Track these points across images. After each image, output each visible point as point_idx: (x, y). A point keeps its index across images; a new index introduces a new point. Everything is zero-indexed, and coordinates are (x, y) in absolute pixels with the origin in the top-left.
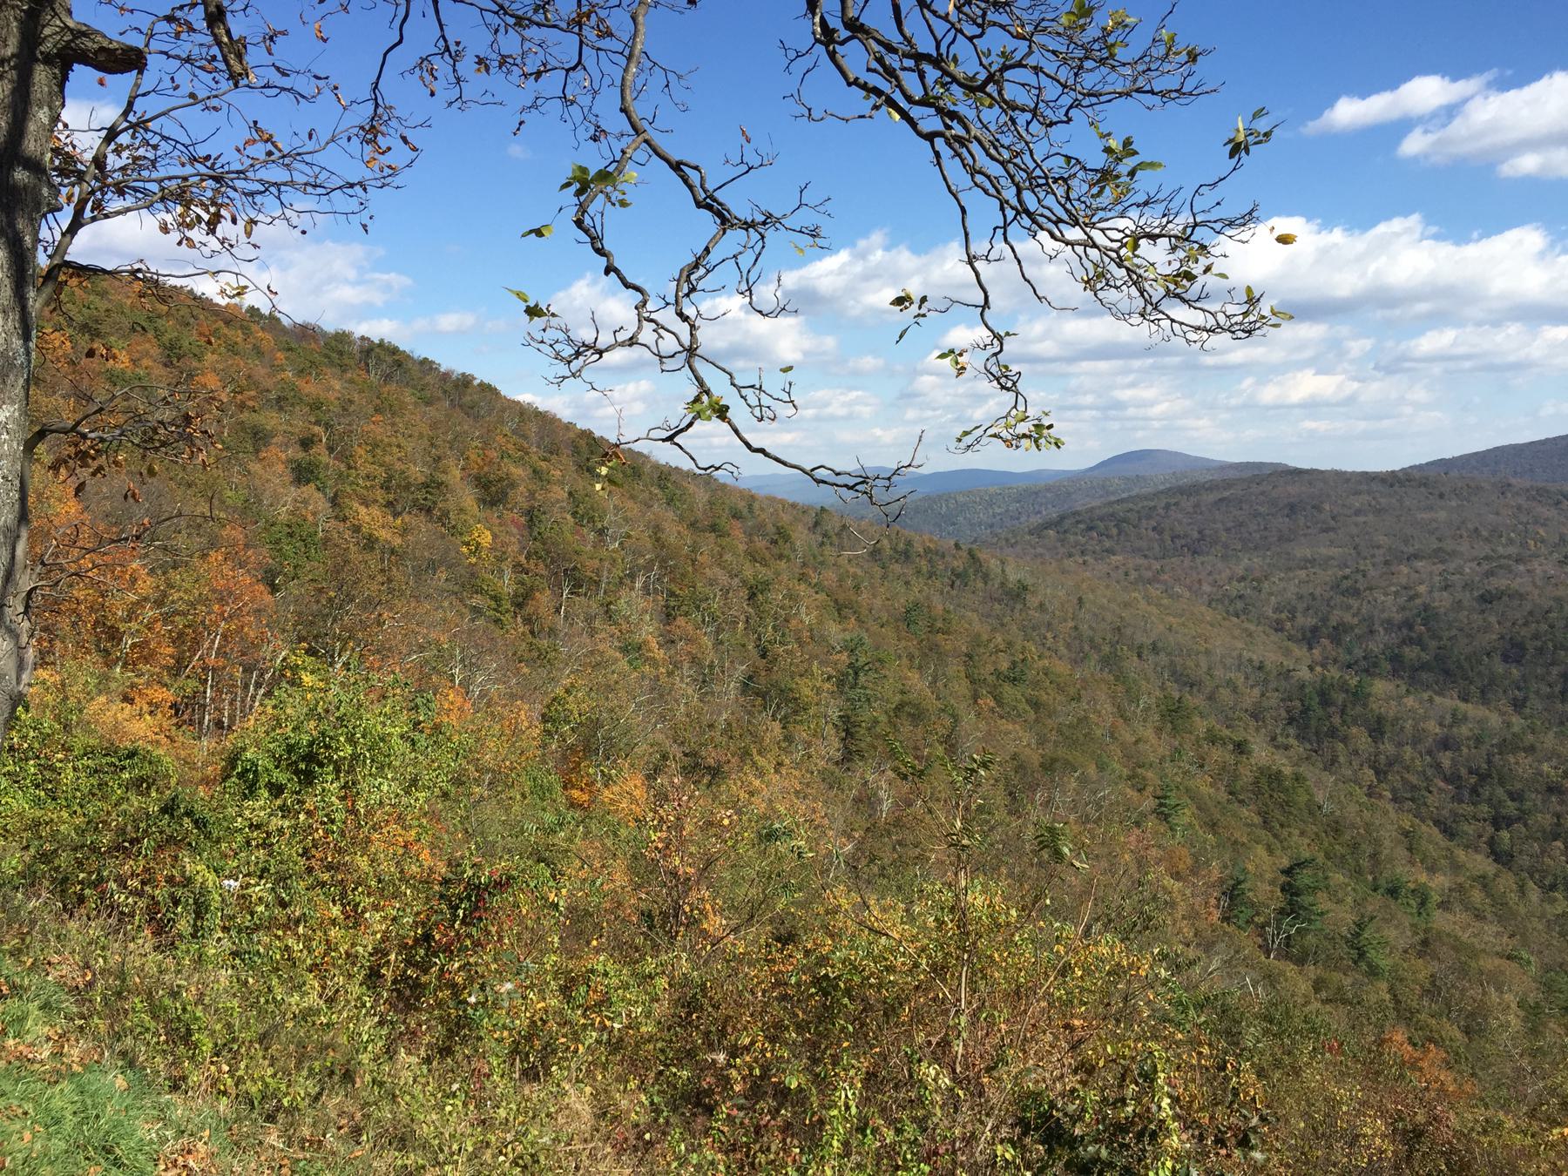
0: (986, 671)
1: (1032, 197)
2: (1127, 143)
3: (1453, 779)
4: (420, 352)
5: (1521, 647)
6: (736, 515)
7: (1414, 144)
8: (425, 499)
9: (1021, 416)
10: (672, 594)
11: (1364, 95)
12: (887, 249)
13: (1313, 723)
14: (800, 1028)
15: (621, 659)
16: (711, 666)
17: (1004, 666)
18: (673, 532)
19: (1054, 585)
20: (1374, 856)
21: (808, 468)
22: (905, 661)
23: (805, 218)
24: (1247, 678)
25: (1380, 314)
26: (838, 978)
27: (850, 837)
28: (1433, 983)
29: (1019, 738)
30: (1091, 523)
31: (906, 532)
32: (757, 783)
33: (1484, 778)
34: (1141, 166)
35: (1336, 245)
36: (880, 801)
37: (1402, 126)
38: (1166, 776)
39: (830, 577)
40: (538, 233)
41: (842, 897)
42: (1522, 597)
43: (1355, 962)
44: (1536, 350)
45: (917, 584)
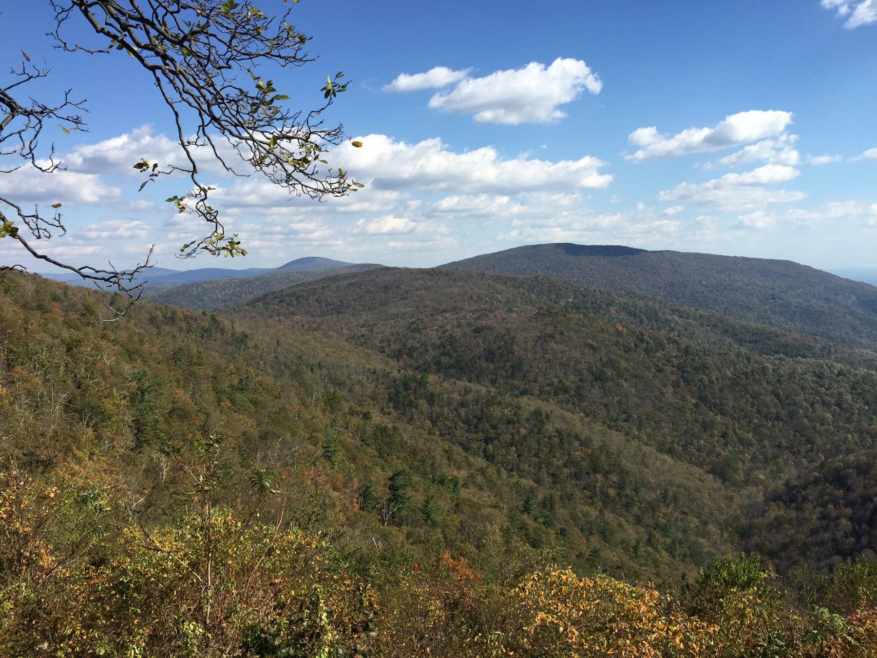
0: (225, 386)
1: (220, 112)
2: (269, 84)
3: (466, 421)
5: (493, 353)
6: (56, 299)
7: (436, 102)
9: (219, 236)
10: (11, 351)
11: (412, 73)
12: (153, 136)
13: (401, 400)
14: (108, 616)
16: (42, 396)
17: (236, 382)
20: (432, 465)
21: (77, 268)
22: (174, 384)
23: (70, 111)
24: (368, 379)
25: (423, 188)
26: (130, 581)
27: (142, 494)
28: (461, 525)
29: (247, 423)
30: (281, 298)
31: (172, 306)
32: (77, 468)
33: (480, 419)
34: (277, 97)
35: (401, 151)
36: (162, 470)
37: (429, 92)
38: (328, 435)
39: (123, 335)
41: (132, 531)
42: (492, 329)
43: (426, 521)
44: (494, 208)
45: (180, 337)
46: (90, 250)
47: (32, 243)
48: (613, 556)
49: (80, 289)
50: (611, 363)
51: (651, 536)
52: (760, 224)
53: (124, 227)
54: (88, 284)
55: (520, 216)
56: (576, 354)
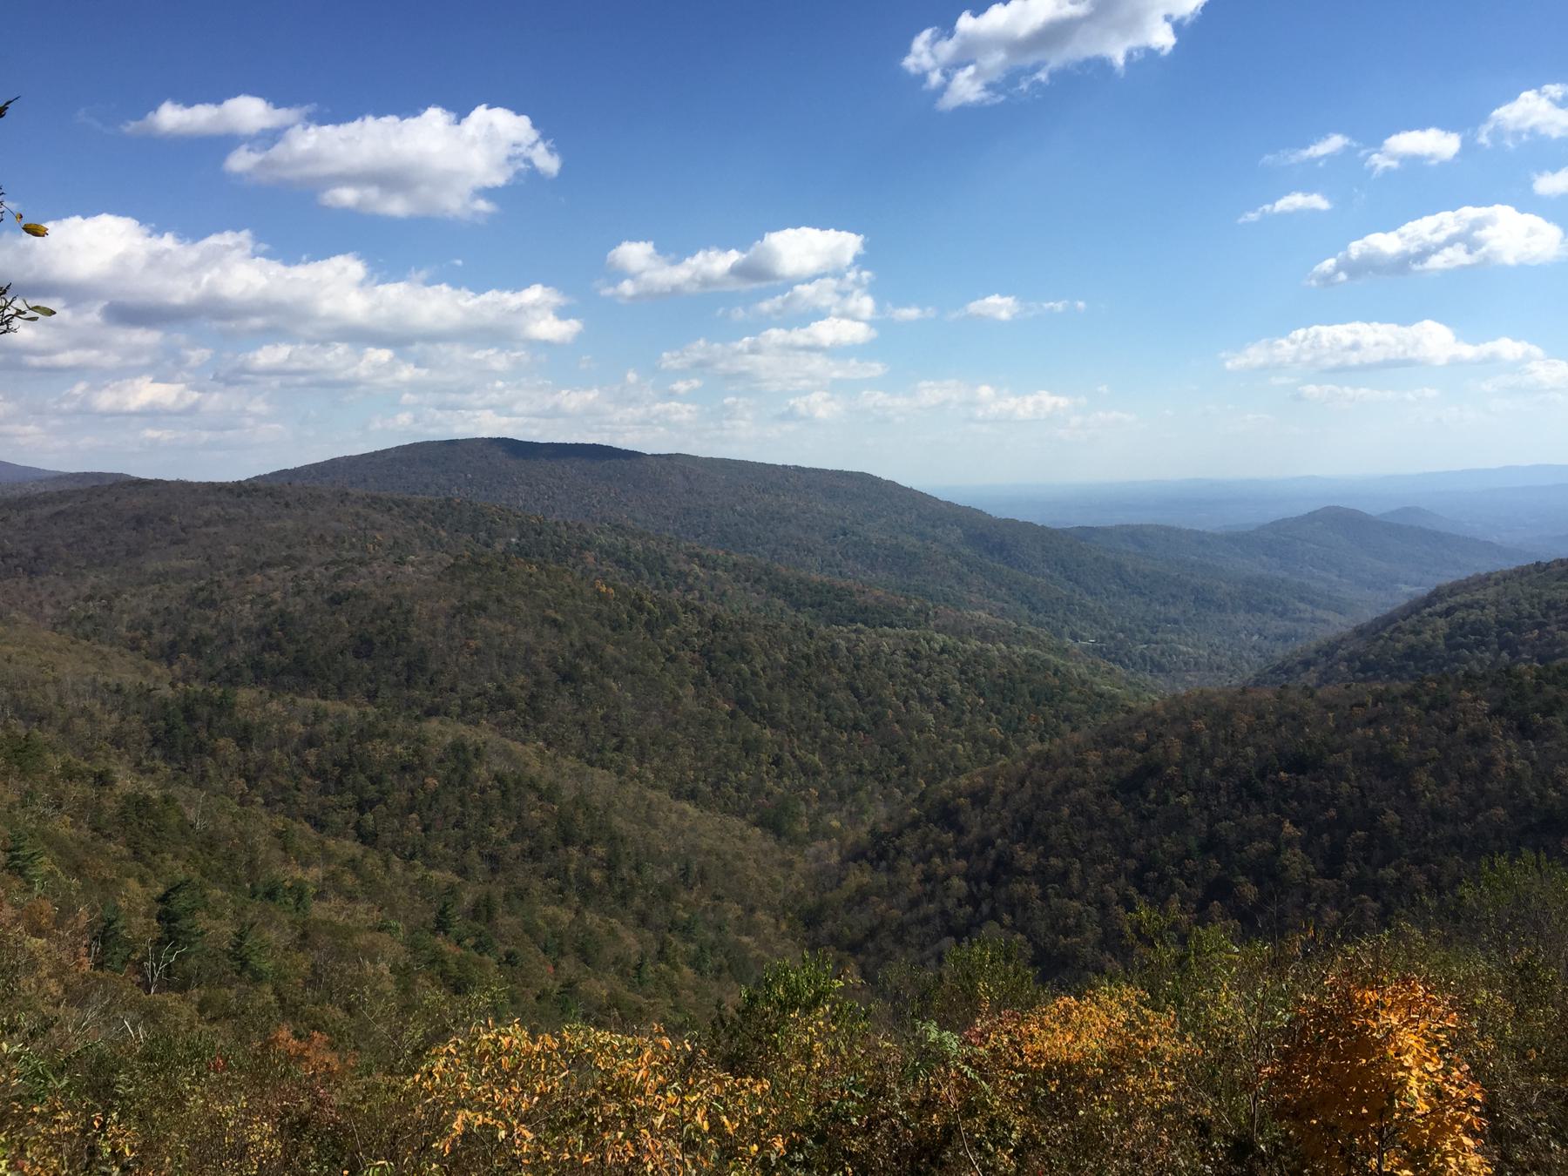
7: (241, 161)
11: (189, 103)
33: (346, 768)
37: (227, 142)
42: (366, 596)
44: (363, 370)
48: (599, 988)
50: (589, 650)
51: (664, 944)
52: (821, 413)
56: (527, 637)
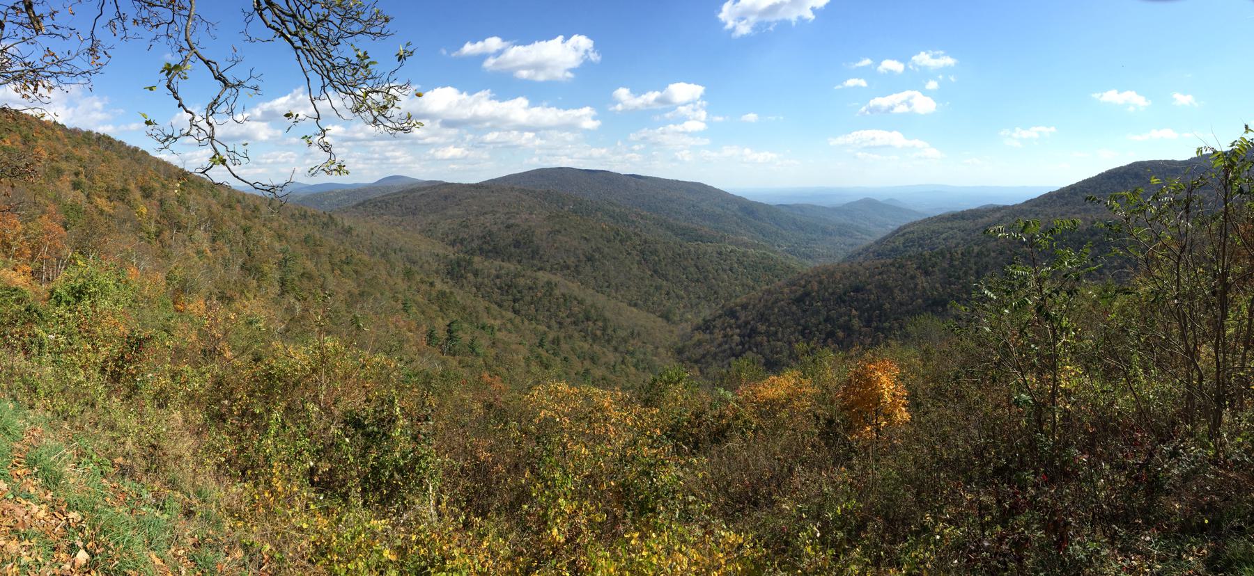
0: (337, 260)
1: (336, 76)
2: (365, 53)
4: (118, 139)
6: (239, 202)
7: (490, 63)
8: (121, 195)
11: (474, 42)
15: (194, 254)
18: (215, 208)
19: (362, 226)
23: (253, 83)
29: (350, 285)
33: (510, 287)
37: (483, 57)
40: (151, 89)
42: (518, 225)
44: (523, 141)
46: (260, 171)
47: (232, 167)
48: (598, 372)
49: (252, 195)
50: (598, 250)
51: (624, 359)
52: (687, 159)
53: (282, 156)
54: (258, 193)
55: (541, 147)
56: (575, 243)
